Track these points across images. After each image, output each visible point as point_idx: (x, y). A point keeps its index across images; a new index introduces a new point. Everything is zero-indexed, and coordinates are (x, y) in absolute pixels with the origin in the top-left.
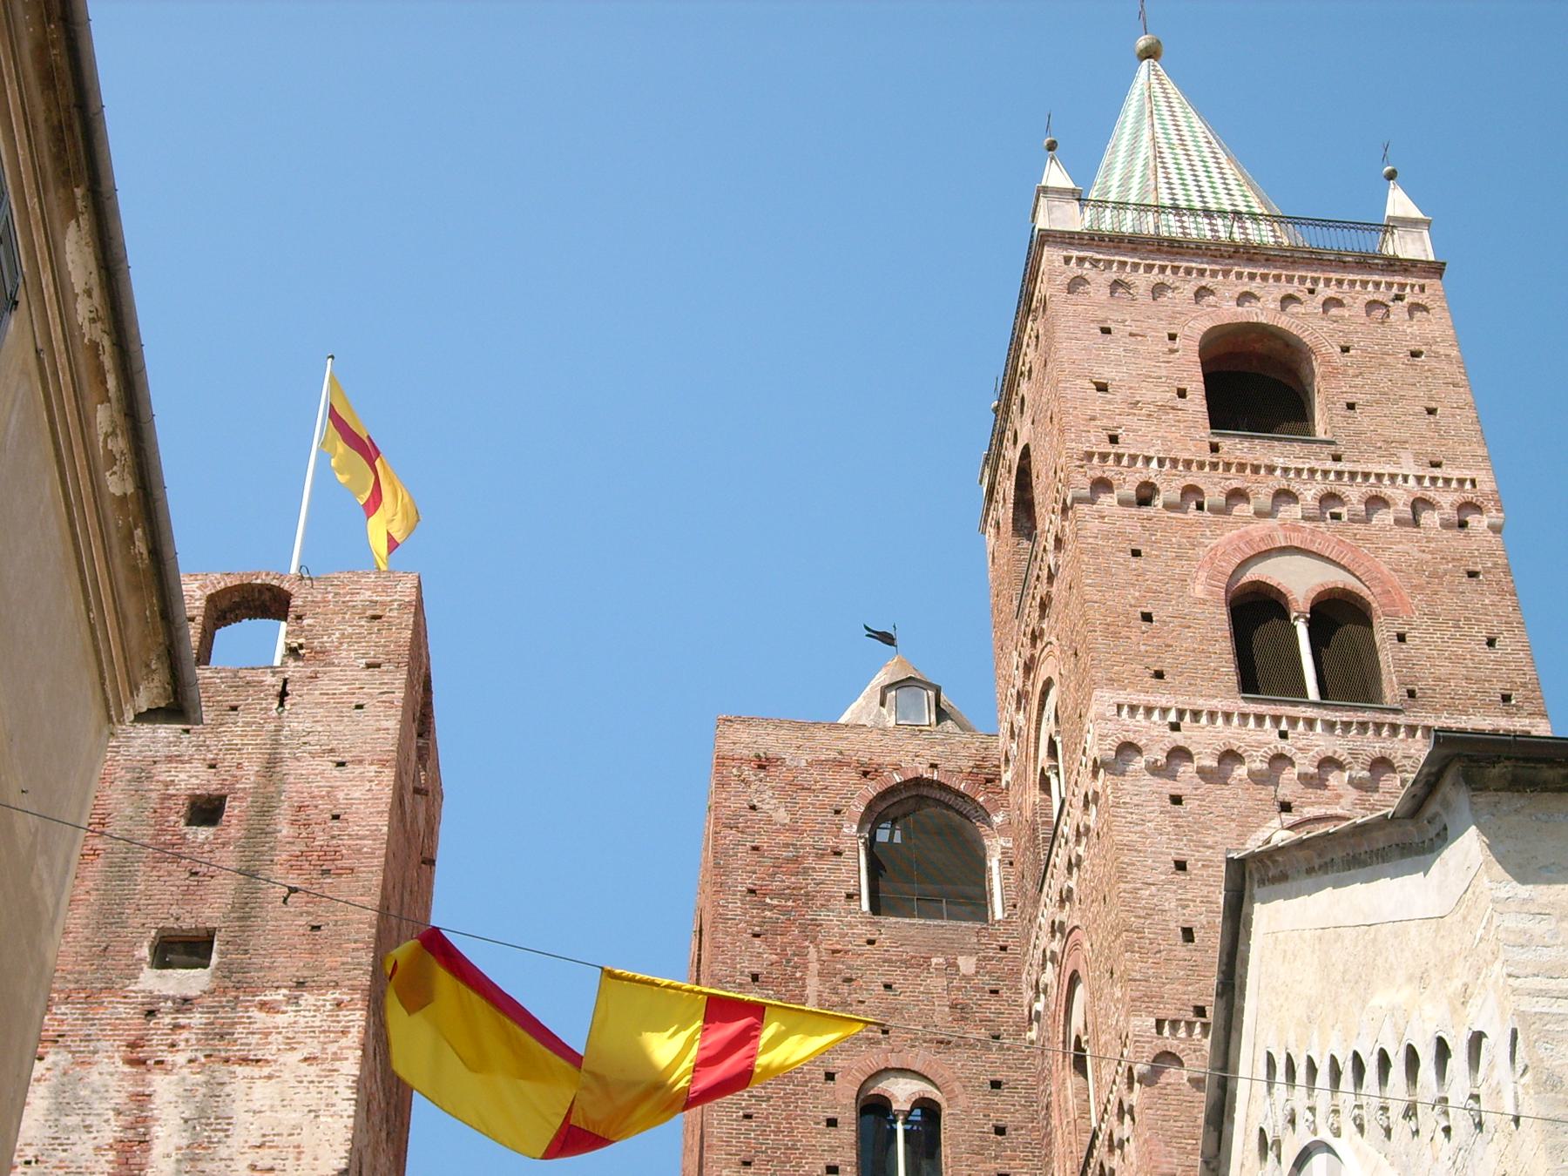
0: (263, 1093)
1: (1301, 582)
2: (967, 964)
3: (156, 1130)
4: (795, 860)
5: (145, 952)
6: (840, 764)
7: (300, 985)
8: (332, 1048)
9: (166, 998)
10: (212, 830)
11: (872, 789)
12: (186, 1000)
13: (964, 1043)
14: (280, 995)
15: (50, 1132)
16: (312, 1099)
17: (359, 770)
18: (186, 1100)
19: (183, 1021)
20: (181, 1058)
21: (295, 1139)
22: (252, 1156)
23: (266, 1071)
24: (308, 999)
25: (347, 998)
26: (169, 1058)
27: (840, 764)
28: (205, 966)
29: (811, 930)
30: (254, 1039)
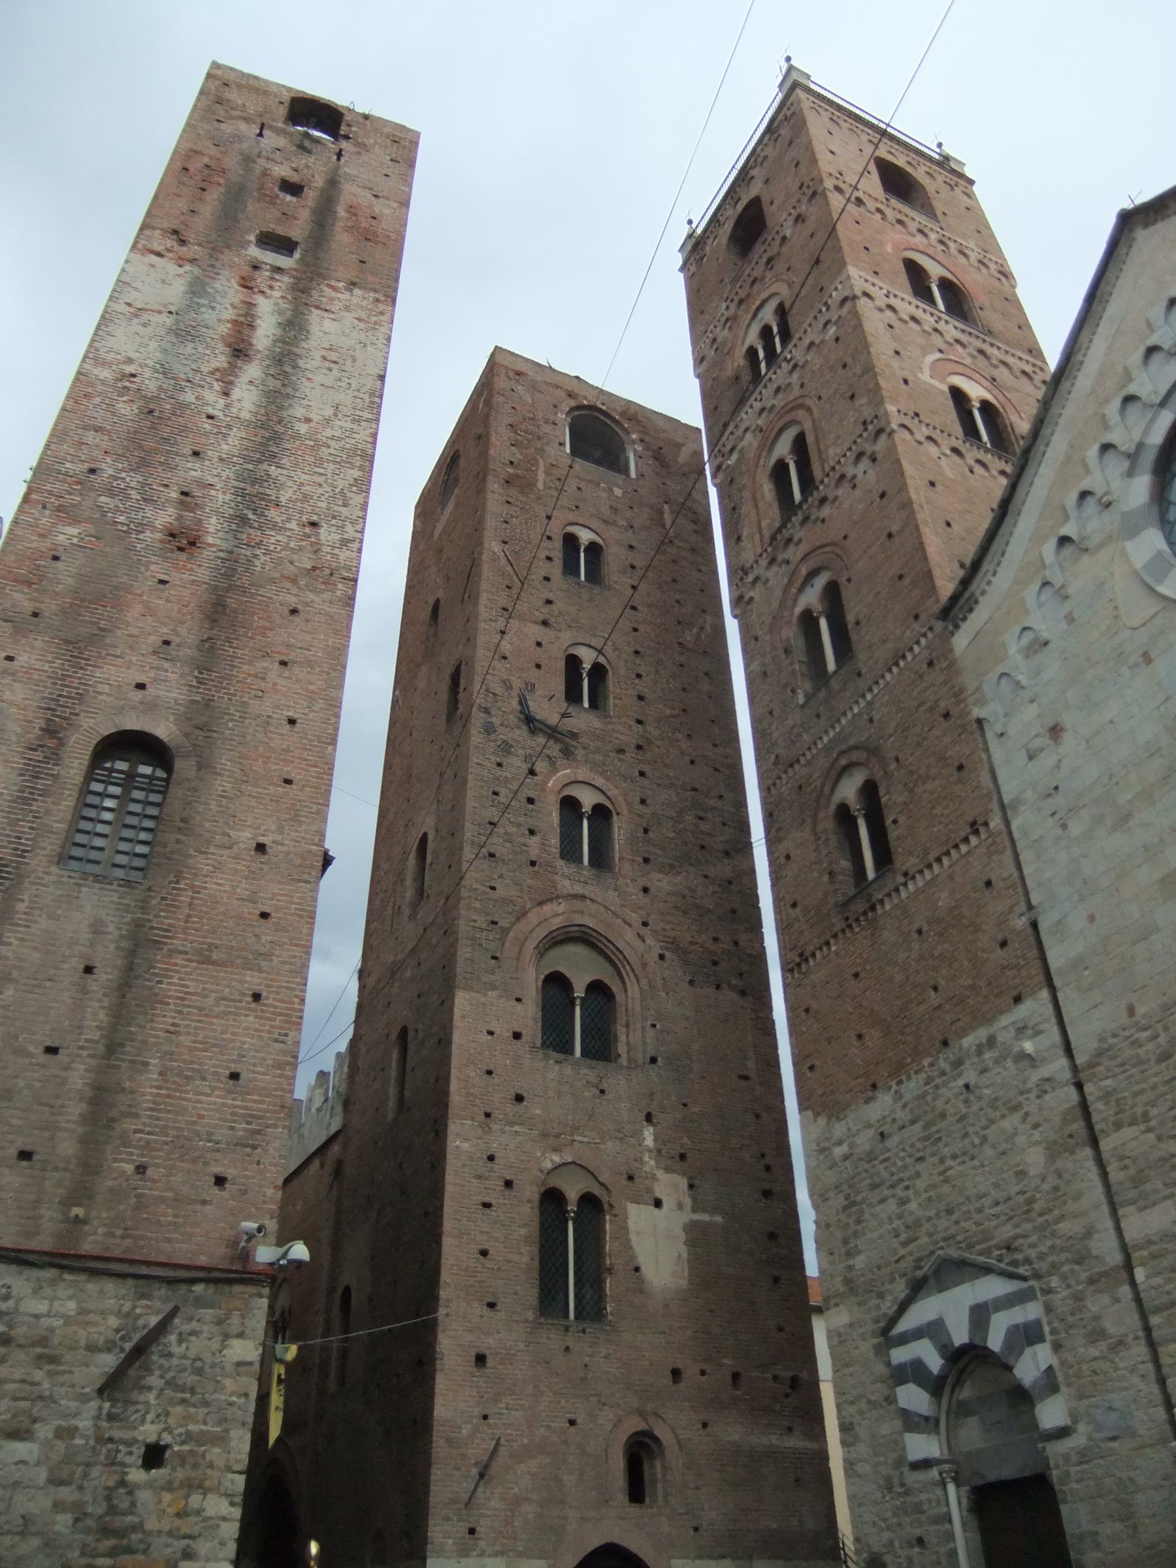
0: (328, 325)
1: (585, 536)
2: (618, 492)
3: (259, 321)
4: (533, 419)
5: (252, 238)
6: (558, 387)
7: (353, 284)
8: (374, 319)
9: (266, 264)
10: (294, 199)
11: (573, 403)
12: (279, 269)
13: (614, 523)
14: (341, 285)
15: (188, 303)
16: (362, 337)
17: (387, 202)
18: (279, 314)
19: (277, 277)
20: (277, 294)
21: (351, 353)
22: (324, 353)
23: (332, 316)
24: (357, 291)
25: (382, 299)
26: (268, 291)
27: (558, 387)
28: (291, 256)
29: (541, 451)
30: (324, 300)
